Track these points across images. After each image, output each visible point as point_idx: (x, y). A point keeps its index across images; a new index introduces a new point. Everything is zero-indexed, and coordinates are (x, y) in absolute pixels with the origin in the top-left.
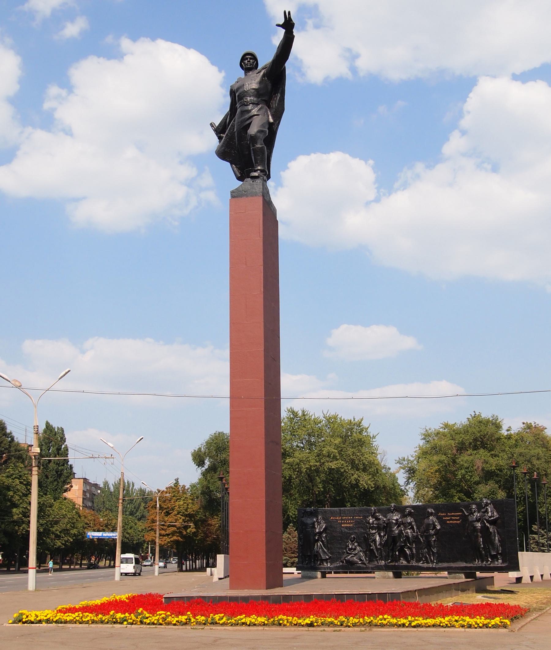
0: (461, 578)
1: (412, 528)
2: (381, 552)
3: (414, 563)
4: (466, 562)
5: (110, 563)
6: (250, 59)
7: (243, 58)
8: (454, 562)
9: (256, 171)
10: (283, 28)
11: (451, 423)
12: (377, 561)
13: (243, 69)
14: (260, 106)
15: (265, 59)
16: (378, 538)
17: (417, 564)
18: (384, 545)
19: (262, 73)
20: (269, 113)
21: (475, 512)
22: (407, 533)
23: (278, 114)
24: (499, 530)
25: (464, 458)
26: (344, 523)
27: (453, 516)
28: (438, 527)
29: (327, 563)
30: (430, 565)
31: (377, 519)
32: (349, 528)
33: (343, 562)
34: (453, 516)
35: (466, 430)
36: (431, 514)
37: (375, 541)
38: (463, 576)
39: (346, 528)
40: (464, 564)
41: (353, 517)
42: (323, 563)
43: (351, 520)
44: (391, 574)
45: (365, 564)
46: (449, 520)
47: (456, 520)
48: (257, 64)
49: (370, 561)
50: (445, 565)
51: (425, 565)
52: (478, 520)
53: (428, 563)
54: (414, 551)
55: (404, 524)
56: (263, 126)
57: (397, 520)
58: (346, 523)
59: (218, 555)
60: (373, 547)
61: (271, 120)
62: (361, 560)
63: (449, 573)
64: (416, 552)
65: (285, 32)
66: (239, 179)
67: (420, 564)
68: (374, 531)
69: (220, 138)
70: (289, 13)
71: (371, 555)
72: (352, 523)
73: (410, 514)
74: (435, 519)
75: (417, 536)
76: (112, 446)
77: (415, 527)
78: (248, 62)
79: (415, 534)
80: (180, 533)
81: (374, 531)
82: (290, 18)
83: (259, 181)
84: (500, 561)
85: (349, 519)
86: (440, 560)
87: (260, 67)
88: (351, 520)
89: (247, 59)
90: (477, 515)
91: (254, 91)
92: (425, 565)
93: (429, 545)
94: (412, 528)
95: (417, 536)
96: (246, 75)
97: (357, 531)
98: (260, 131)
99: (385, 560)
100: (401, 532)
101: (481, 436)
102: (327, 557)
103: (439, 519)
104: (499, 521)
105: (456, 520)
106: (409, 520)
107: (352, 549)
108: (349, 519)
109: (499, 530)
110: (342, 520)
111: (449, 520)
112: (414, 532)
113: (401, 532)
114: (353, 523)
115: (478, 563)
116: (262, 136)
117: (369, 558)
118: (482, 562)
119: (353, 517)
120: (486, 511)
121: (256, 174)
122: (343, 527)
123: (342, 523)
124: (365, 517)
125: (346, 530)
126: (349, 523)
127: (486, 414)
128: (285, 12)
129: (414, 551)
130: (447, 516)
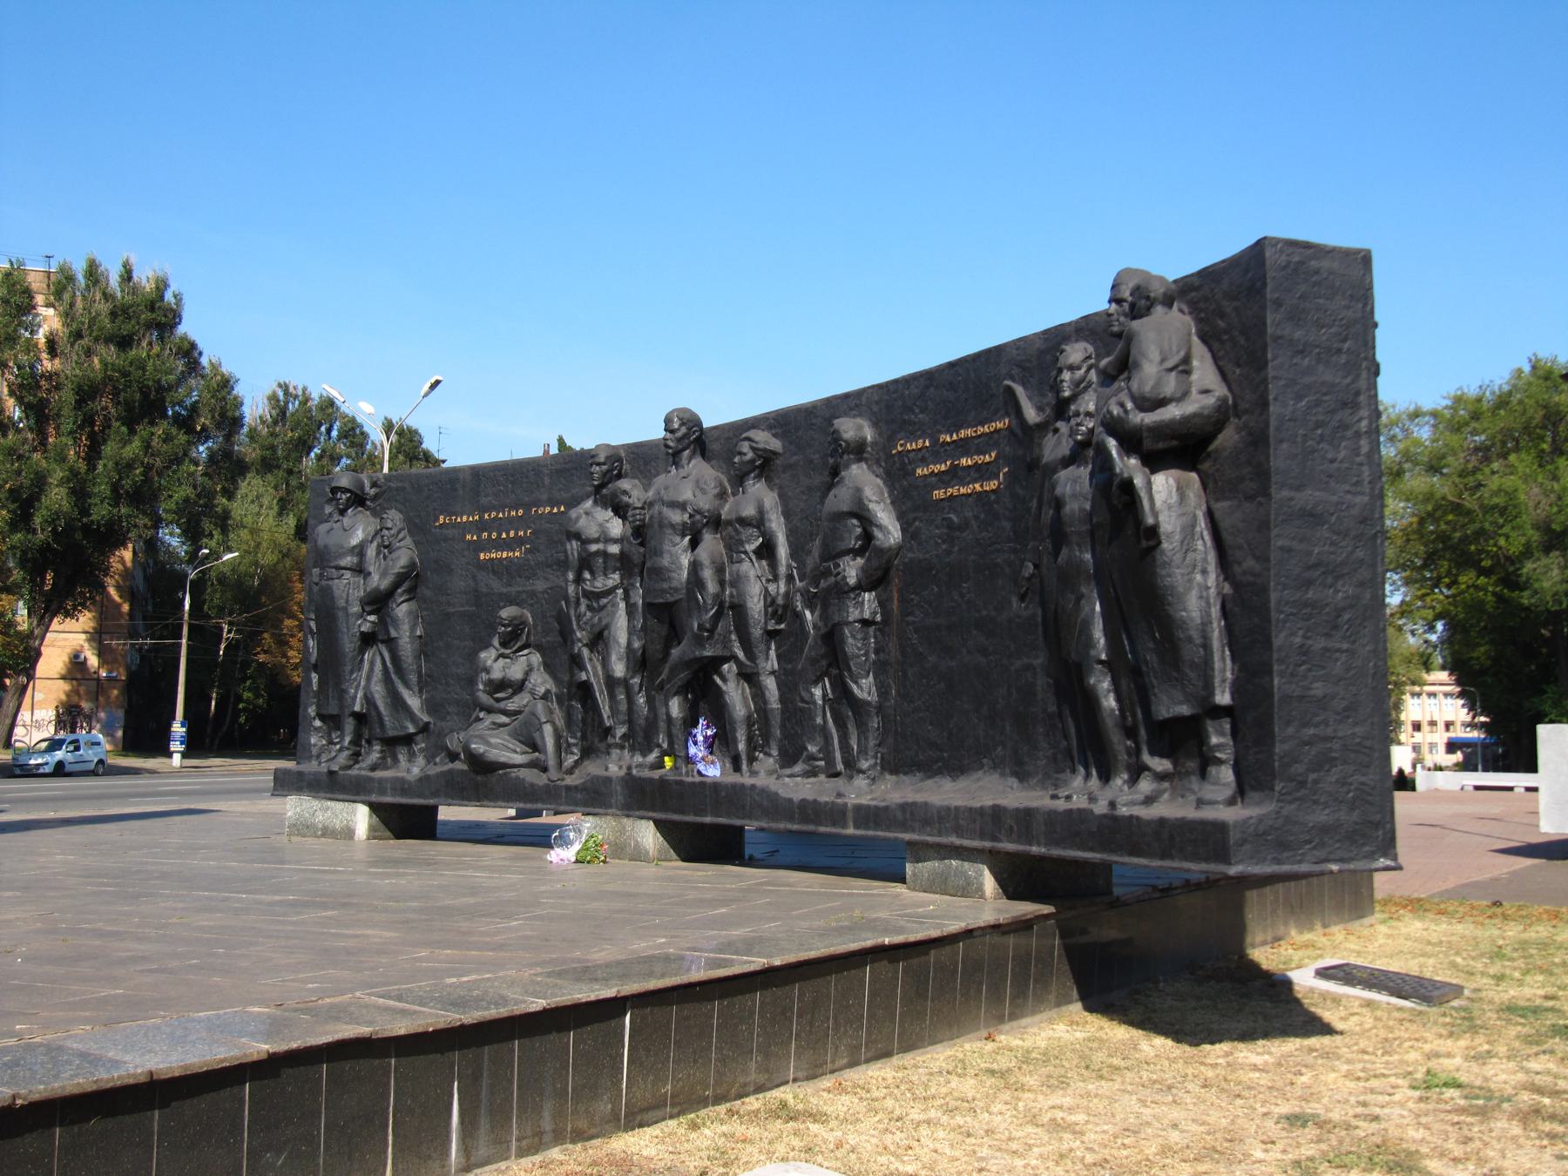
24: (1220, 507)
25: (1496, 480)
27: (964, 447)
34: (964, 447)
36: (858, 450)
38: (989, 883)
39: (494, 567)
42: (396, 760)
46: (945, 479)
47: (982, 472)
54: (770, 684)
59: (1543, 730)
60: (592, 672)
72: (519, 542)
73: (765, 465)
77: (783, 551)
81: (600, 584)
88: (512, 523)
102: (412, 730)
103: (897, 475)
104: (1228, 438)
105: (982, 472)
107: (501, 685)
108: (510, 520)
109: (1220, 507)
110: (481, 526)
111: (945, 479)
114: (519, 542)
119: (528, 507)
123: (479, 546)
129: (770, 684)
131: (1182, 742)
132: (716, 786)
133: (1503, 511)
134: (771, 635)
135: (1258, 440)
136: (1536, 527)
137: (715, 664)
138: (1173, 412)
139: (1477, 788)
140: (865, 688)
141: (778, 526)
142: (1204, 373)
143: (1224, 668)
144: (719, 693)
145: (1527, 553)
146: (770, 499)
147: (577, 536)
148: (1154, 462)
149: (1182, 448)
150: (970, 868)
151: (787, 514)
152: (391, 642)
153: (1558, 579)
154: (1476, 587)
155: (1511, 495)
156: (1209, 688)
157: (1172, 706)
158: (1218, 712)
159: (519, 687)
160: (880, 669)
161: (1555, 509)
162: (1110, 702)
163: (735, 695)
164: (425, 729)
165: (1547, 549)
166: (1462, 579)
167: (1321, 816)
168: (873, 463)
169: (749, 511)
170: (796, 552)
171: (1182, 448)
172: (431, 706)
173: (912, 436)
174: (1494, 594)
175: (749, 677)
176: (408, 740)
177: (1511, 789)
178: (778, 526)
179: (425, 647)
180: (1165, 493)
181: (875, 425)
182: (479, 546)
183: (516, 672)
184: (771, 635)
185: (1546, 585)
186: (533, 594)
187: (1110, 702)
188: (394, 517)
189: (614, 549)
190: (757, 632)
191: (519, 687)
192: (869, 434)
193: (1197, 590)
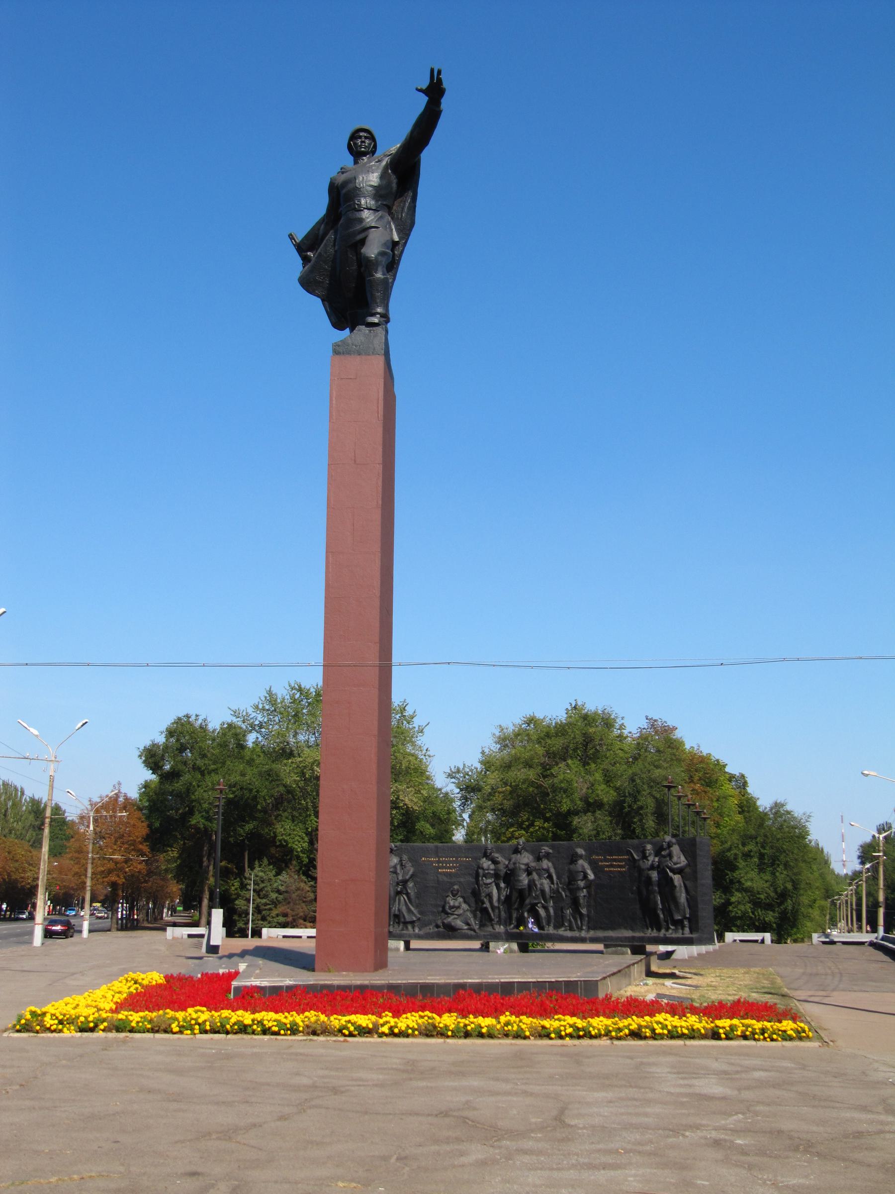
0: (629, 957)
1: (550, 877)
2: (500, 912)
3: (551, 930)
4: (633, 930)
5: (10, 915)
6: (366, 138)
7: (354, 136)
8: (613, 928)
9: (373, 315)
10: (427, 95)
11: (539, 715)
12: (492, 925)
13: (351, 154)
14: (380, 213)
15: (390, 143)
16: (495, 891)
17: (555, 932)
18: (508, 901)
19: (384, 163)
20: (393, 227)
21: (650, 855)
22: (542, 884)
23: (406, 229)
26: (443, 867)
27: (615, 860)
28: (591, 876)
29: (413, 928)
30: (576, 934)
31: (495, 862)
32: (449, 875)
33: (437, 926)
34: (615, 860)
35: (561, 730)
37: (490, 896)
38: (629, 952)
39: (445, 874)
40: (628, 933)
41: (457, 858)
42: (407, 928)
43: (453, 862)
44: (515, 946)
45: (474, 931)
46: (607, 866)
48: (375, 147)
49: (482, 925)
50: (600, 934)
51: (569, 934)
52: (652, 867)
53: (571, 929)
54: (552, 911)
55: (539, 871)
56: (385, 244)
57: (527, 865)
58: (446, 868)
61: (396, 238)
62: (468, 924)
63: (606, 946)
64: (555, 913)
65: (428, 103)
66: (338, 324)
67: (583, 934)
68: (489, 881)
69: (306, 260)
70: (439, 72)
71: (484, 916)
72: (454, 867)
74: (586, 865)
75: (558, 889)
76: (36, 732)
78: (360, 145)
79: (554, 887)
80: (121, 869)
81: (489, 881)
82: (440, 81)
83: (379, 330)
84: (687, 930)
85: (450, 862)
86: (594, 925)
87: (379, 153)
88: (453, 862)
89: (360, 137)
90: (653, 859)
91: (371, 189)
92: (569, 934)
93: (575, 904)
94: (550, 877)
95: (558, 889)
96: (356, 162)
97: (462, 880)
98: (382, 254)
99: (505, 925)
100: (532, 884)
101: (583, 738)
102: (415, 919)
103: (594, 865)
106: (546, 864)
107: (453, 907)
108: (450, 862)
109: (686, 882)
111: (607, 866)
112: (553, 883)
113: (532, 884)
114: (454, 867)
115: (651, 933)
116: (384, 261)
117: (481, 921)
118: (659, 930)
120: (670, 855)
121: (375, 320)
122: (441, 873)
123: (439, 868)
124: (476, 859)
125: (445, 879)
126: (450, 868)
127: (592, 704)
128: (432, 71)
129: (552, 911)
130: (606, 860)
131: (679, 924)
132: (536, 933)
133: (565, 791)
134: (551, 897)
135: (695, 872)
136: (581, 799)
137: (536, 904)
138: (678, 866)
139: (284, 937)
140: (584, 911)
141: (552, 870)
142: (683, 858)
143: (688, 911)
144: (537, 911)
145: (576, 813)
146: (550, 864)
147: (483, 869)
148: (675, 874)
149: (680, 871)
150: (624, 949)
151: (555, 868)
152: (408, 894)
153: (591, 828)
154: (544, 828)
155: (569, 782)
156: (685, 914)
157: (678, 917)
158: (686, 918)
159: (458, 907)
160: (588, 907)
161: (590, 791)
162: (662, 916)
163: (542, 912)
164: (419, 919)
165: (585, 812)
166: (537, 823)
167: (705, 936)
168: (585, 860)
169: (545, 867)
170: (558, 878)
171: (680, 871)
172: (421, 913)
173: (598, 855)
174: (553, 832)
175: (545, 908)
176: (412, 923)
177: (300, 937)
178: (552, 870)
179: (418, 896)
180: (677, 879)
181: (585, 851)
182: (439, 868)
183: (457, 904)
184: (551, 897)
185: (586, 831)
186: (460, 882)
187: (662, 916)
188: (405, 857)
189: (492, 872)
190: (548, 896)
191: (458, 907)
192: (583, 853)
193: (682, 898)
